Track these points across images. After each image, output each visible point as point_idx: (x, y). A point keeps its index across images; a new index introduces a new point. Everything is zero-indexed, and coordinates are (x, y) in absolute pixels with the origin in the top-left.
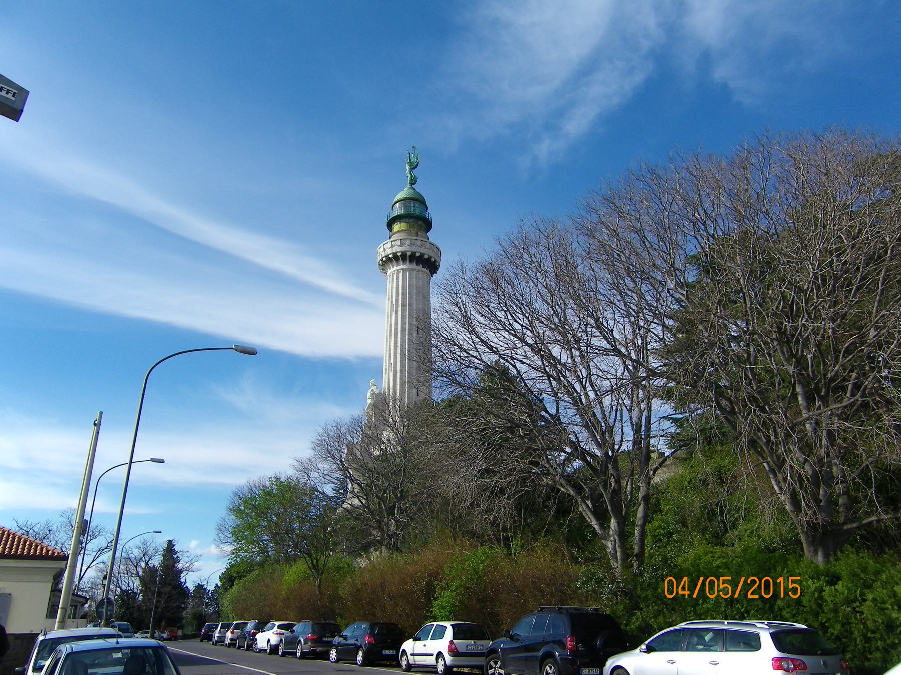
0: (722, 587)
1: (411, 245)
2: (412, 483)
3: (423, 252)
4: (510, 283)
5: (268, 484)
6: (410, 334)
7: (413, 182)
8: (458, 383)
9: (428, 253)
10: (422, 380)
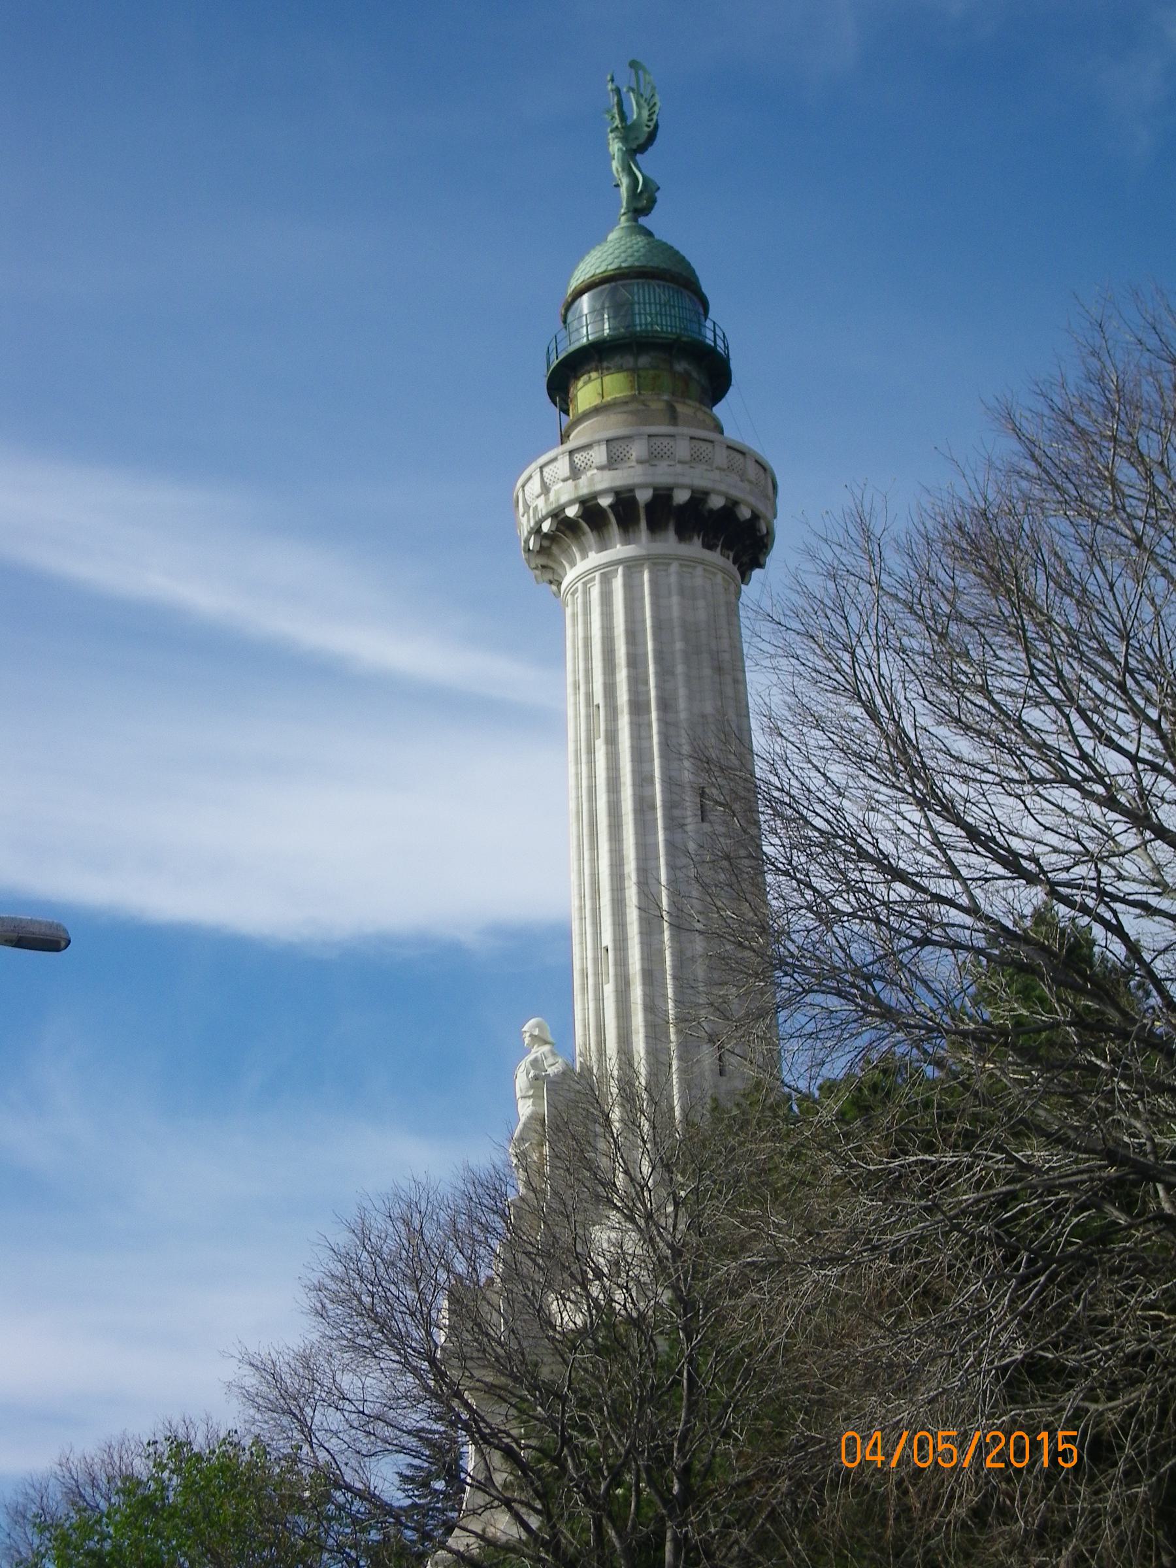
0: (941, 1448)
1: (651, 459)
2: (726, 1435)
3: (736, 493)
4: (1066, 585)
5: (141, 1468)
6: (673, 825)
7: (642, 203)
8: (887, 1013)
9: (721, 486)
10: (738, 1009)
